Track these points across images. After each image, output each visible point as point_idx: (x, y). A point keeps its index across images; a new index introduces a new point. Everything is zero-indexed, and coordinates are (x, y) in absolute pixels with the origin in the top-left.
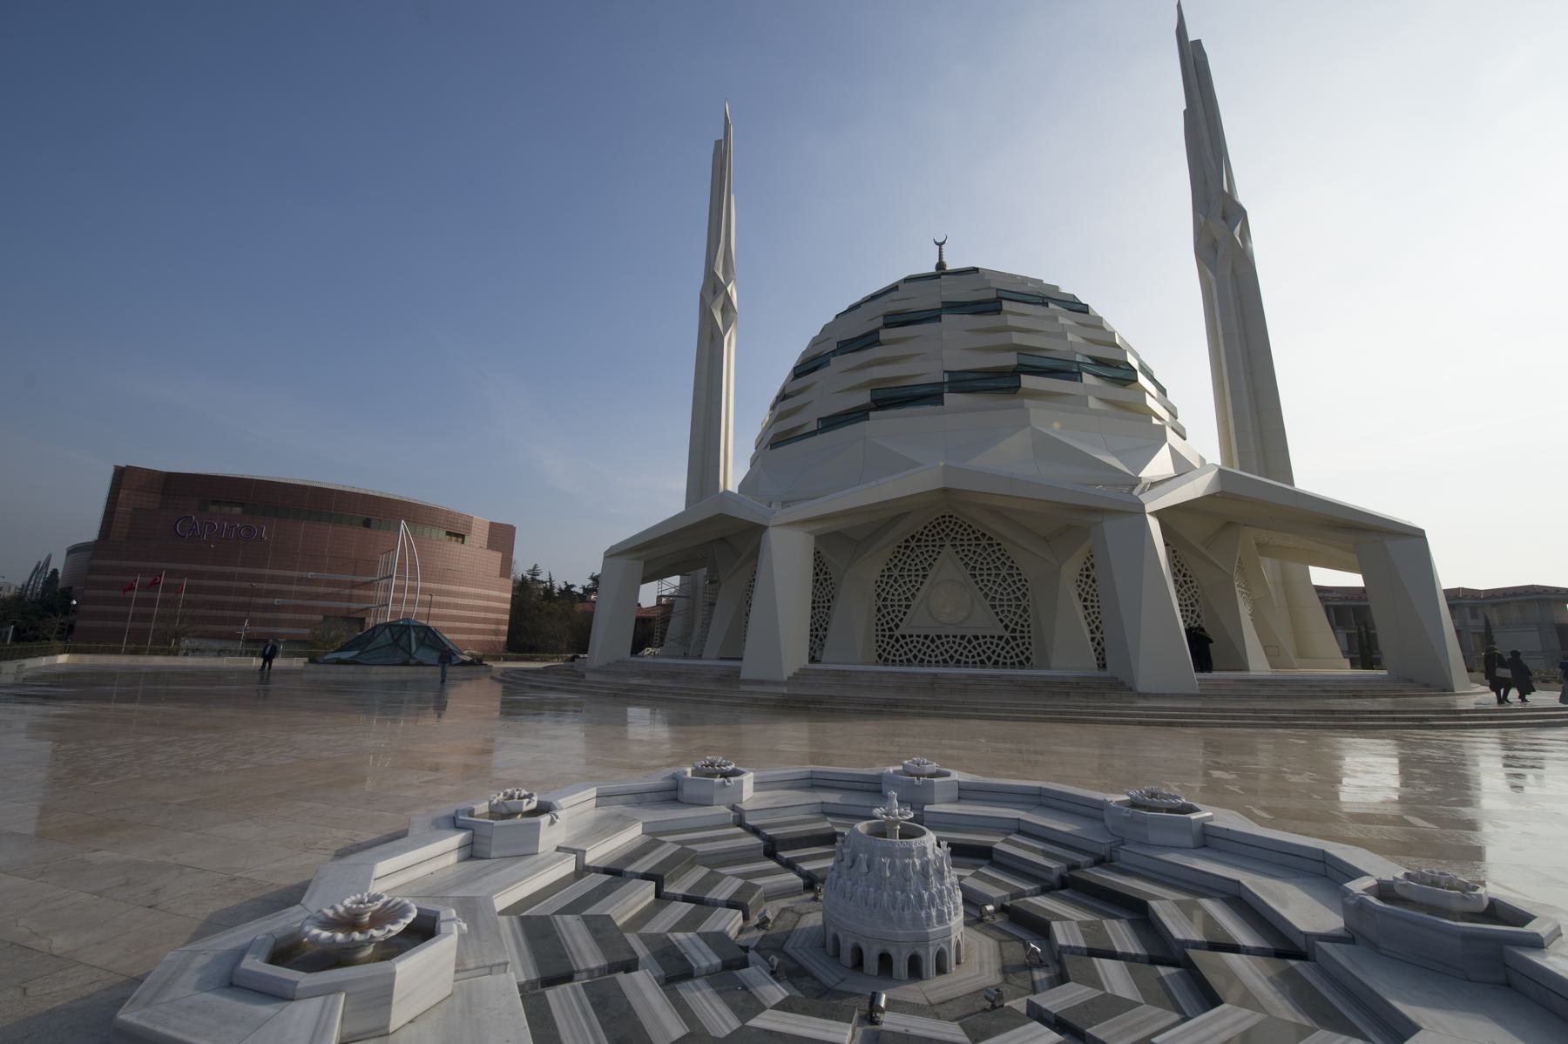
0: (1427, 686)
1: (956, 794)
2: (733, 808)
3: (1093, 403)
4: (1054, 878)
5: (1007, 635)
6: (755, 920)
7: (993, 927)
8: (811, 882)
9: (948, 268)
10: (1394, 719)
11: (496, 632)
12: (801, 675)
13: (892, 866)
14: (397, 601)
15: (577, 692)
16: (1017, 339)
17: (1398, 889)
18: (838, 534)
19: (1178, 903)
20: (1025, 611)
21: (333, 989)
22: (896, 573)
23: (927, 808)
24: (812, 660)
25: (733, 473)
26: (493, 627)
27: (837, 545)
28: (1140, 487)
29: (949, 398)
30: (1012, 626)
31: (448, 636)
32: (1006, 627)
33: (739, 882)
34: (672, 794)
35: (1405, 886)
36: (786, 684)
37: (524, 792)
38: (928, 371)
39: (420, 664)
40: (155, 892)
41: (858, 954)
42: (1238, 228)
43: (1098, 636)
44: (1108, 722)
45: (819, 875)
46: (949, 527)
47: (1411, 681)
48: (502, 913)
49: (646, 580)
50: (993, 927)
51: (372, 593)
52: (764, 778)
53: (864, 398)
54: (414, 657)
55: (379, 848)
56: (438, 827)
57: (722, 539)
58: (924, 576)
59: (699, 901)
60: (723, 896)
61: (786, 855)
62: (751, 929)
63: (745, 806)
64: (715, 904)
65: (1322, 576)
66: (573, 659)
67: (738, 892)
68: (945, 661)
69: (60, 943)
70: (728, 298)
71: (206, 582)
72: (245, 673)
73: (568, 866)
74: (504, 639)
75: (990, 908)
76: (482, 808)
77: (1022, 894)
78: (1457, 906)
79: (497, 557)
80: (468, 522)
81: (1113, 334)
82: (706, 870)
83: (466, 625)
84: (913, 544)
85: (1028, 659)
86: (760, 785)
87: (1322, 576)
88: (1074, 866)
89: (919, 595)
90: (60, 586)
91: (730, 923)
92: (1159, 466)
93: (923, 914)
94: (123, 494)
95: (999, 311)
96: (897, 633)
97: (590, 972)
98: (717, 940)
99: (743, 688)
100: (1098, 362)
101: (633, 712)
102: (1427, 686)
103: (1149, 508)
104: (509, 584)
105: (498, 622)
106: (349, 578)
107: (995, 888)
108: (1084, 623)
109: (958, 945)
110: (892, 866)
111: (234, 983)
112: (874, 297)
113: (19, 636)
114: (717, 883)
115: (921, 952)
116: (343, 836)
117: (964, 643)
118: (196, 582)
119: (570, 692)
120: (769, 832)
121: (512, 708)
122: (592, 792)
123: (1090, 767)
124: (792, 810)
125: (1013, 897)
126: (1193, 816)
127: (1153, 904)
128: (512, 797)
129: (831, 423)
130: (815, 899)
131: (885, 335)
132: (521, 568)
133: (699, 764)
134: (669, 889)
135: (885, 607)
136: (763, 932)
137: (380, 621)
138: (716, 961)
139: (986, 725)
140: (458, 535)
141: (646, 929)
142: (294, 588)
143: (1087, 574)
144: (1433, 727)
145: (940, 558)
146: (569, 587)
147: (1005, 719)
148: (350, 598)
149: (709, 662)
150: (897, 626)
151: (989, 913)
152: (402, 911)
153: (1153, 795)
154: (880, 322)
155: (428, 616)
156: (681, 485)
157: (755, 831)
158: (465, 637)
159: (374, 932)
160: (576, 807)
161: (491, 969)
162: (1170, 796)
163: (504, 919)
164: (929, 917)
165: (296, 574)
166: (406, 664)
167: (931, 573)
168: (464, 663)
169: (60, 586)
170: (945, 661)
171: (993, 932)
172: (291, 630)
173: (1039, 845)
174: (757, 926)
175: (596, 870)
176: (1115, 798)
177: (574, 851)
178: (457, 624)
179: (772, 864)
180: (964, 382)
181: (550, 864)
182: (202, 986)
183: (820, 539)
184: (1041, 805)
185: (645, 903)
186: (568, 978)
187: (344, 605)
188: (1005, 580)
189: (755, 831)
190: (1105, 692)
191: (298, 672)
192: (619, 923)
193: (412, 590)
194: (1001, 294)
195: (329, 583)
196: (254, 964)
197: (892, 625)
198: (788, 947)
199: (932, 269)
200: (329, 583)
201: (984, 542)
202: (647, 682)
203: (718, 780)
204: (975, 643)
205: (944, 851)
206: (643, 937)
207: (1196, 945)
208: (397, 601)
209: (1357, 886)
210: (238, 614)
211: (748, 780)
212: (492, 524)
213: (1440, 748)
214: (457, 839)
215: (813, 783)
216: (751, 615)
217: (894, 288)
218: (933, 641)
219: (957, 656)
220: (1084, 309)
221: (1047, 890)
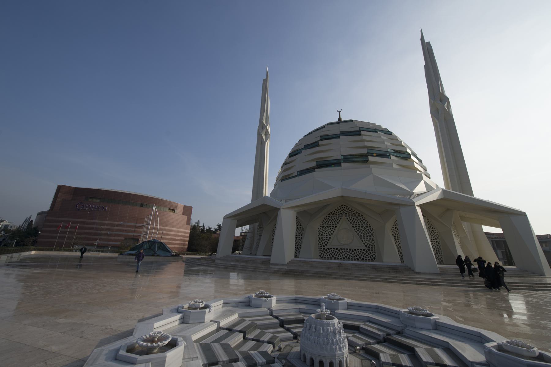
0: (534, 273)
1: (347, 306)
2: (269, 309)
3: (395, 166)
4: (381, 338)
5: (366, 249)
6: (277, 348)
7: (359, 355)
8: (296, 336)
9: (342, 120)
10: (518, 286)
11: (184, 245)
12: (292, 262)
13: (323, 329)
14: (151, 233)
15: (213, 267)
16: (367, 144)
17: (504, 347)
18: (304, 211)
19: (425, 349)
20: (373, 240)
21: (147, 361)
22: (325, 226)
23: (336, 311)
24: (296, 257)
25: (268, 189)
26: (183, 242)
27: (304, 216)
28: (413, 196)
29: (343, 164)
30: (368, 246)
31: (168, 245)
32: (366, 246)
33: (271, 335)
34: (248, 304)
35: (506, 345)
36: (286, 265)
37: (200, 301)
38: (335, 155)
39: (158, 256)
40: (82, 332)
41: (312, 360)
42: (446, 104)
43: (400, 250)
44: (405, 283)
45: (299, 334)
46: (344, 210)
47: (527, 271)
48: (195, 341)
49: (238, 226)
50: (359, 355)
51: (142, 230)
52: (279, 298)
53: (314, 164)
54: (147, 254)
55: (153, 319)
56: (172, 312)
57: (264, 213)
58: (336, 227)
59: (258, 341)
60: (266, 340)
61: (287, 326)
62: (275, 351)
63: (273, 309)
64: (263, 342)
65: (487, 229)
66: (211, 255)
67: (271, 338)
68: (344, 258)
69: (54, 348)
70: (267, 130)
71: (85, 226)
72: (75, 258)
73: (214, 327)
74: (186, 247)
75: (358, 348)
76: (186, 306)
77: (370, 343)
78: (526, 354)
79: (186, 217)
80: (176, 205)
81: (401, 142)
82: (260, 331)
83: (174, 242)
84: (331, 215)
85: (374, 258)
86: (278, 301)
87: (487, 229)
88: (389, 334)
89: (334, 234)
90: (33, 226)
91: (269, 348)
92: (420, 188)
93: (334, 347)
94: (60, 194)
95: (360, 134)
96: (326, 247)
97: (223, 361)
98: (264, 354)
99: (271, 266)
100: (396, 151)
101: (233, 275)
102: (534, 273)
103: (416, 204)
104: (189, 227)
105: (185, 241)
106: (134, 224)
107: (360, 341)
108: (395, 245)
109: (346, 359)
110: (323, 329)
111: (117, 358)
112: (317, 130)
113: (17, 244)
114: (264, 335)
115: (334, 361)
116: (140, 315)
117: (351, 251)
118: (81, 225)
119: (210, 267)
120: (281, 318)
121: (188, 272)
122: (221, 302)
123: (396, 299)
124: (289, 311)
125: (366, 344)
126: (431, 318)
127: (416, 349)
128: (196, 302)
129: (302, 173)
130: (297, 342)
131: (320, 143)
132: (194, 222)
133: (257, 293)
134: (248, 336)
135: (322, 238)
136: (279, 353)
137: (144, 240)
138: (264, 361)
139: (359, 283)
140: (172, 210)
141: (241, 349)
142: (116, 228)
143: (395, 227)
144: (535, 290)
145: (340, 223)
146: (210, 228)
147: (366, 280)
148: (134, 232)
149: (259, 257)
150: (326, 245)
151: (358, 350)
152: (167, 337)
153: (417, 309)
154: (319, 138)
155: (161, 238)
156: (250, 192)
157: (276, 317)
158: (173, 246)
159: (159, 343)
160: (217, 307)
161: (193, 359)
162: (423, 310)
163: (195, 344)
164: (336, 348)
165: (116, 223)
166: (153, 255)
167: (338, 226)
168: (173, 256)
169: (33, 226)
170: (344, 258)
171: (360, 357)
172: (113, 243)
173: (376, 326)
174: (278, 351)
175: (223, 329)
176: (403, 310)
177: (216, 322)
178: (171, 241)
179: (282, 329)
180: (348, 159)
181: (208, 326)
182: (107, 360)
183: (298, 213)
184: (377, 312)
185: (239, 342)
186: (216, 363)
187: (132, 234)
188: (365, 229)
189: (276, 317)
190: (403, 272)
191: (116, 258)
192: (232, 347)
193: (156, 229)
194: (361, 129)
195: (127, 226)
196: (123, 352)
197: (324, 244)
198: (288, 358)
199: (337, 120)
200: (127, 226)
201: (357, 215)
202: (237, 263)
203: (264, 299)
204: (355, 252)
205: (341, 325)
206: (240, 352)
207: (431, 364)
208: (151, 233)
209: (489, 345)
210: (95, 237)
211: (274, 299)
212: (184, 206)
213: (536, 298)
214: (178, 316)
215: (296, 301)
216: (274, 240)
217: (323, 127)
218: (339, 251)
219: (335, 256)
220: (391, 133)
221: (379, 342)
